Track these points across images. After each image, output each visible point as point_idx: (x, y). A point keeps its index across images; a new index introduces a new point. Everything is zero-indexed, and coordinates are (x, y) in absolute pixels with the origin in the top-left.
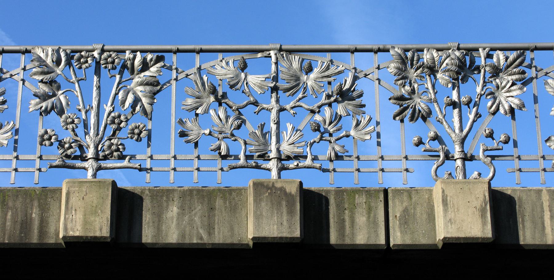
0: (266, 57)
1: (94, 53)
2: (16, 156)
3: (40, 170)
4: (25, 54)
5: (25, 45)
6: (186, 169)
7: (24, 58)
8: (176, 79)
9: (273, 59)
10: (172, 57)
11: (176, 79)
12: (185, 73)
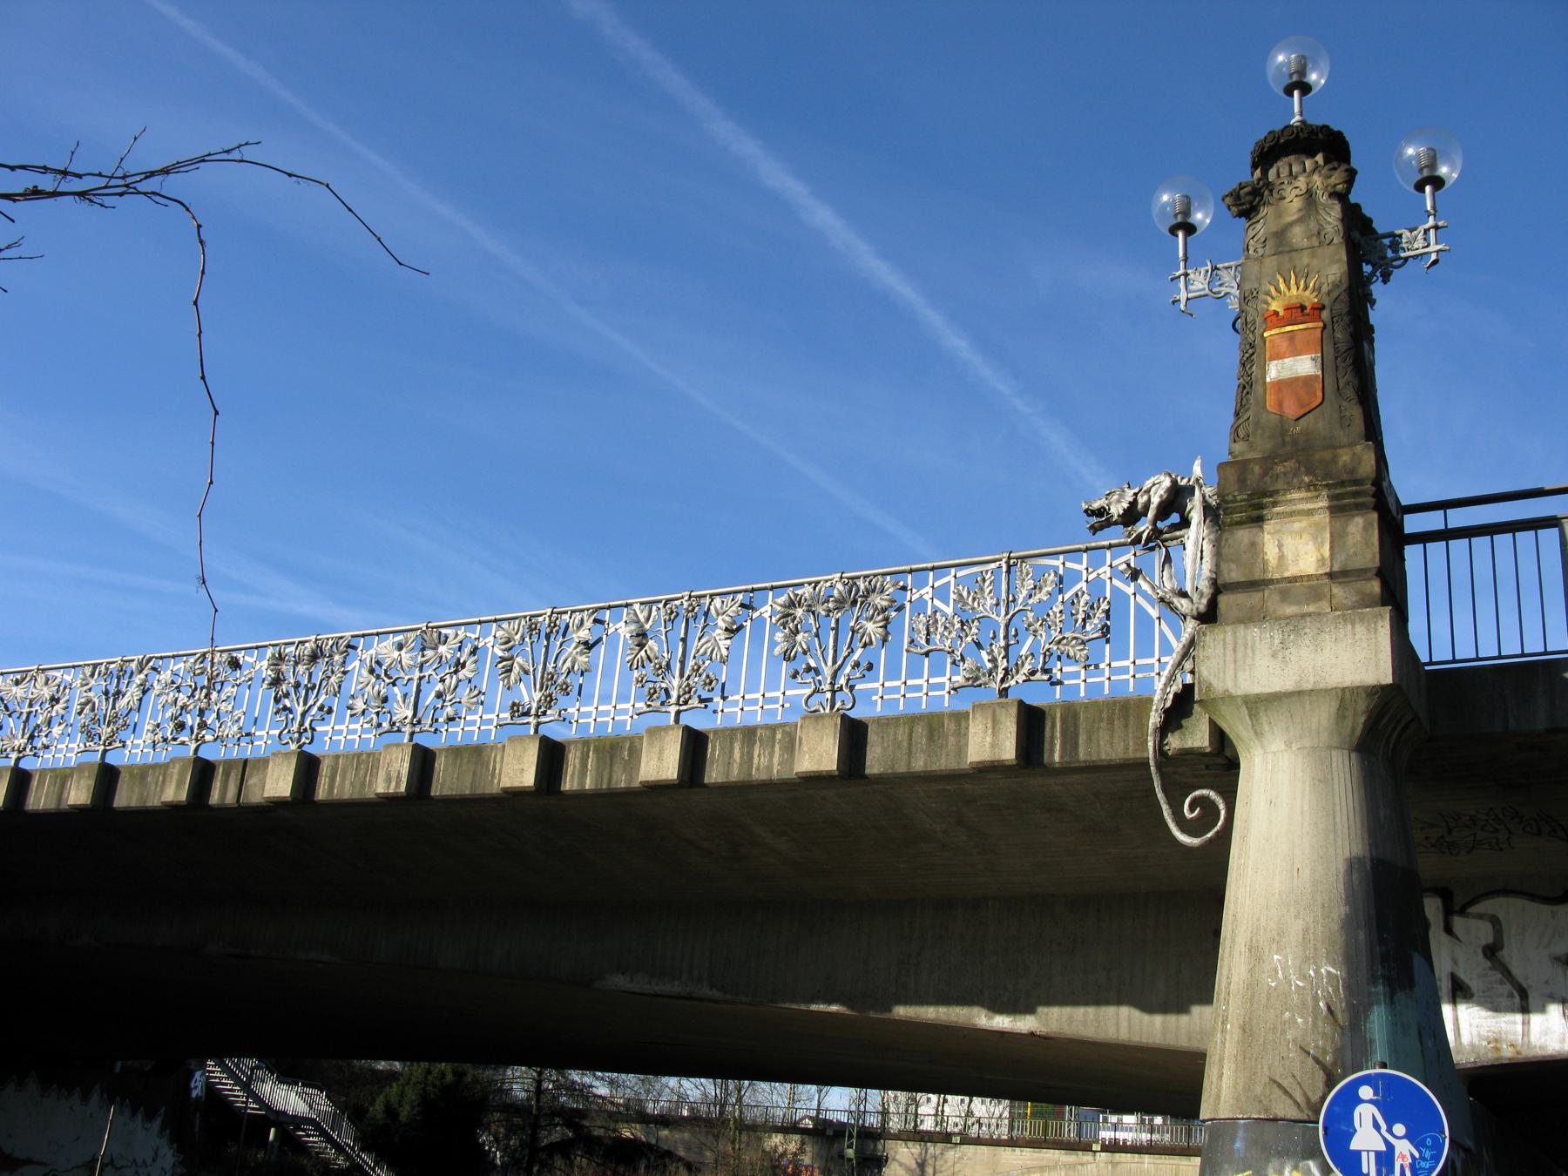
9: (1004, 569)
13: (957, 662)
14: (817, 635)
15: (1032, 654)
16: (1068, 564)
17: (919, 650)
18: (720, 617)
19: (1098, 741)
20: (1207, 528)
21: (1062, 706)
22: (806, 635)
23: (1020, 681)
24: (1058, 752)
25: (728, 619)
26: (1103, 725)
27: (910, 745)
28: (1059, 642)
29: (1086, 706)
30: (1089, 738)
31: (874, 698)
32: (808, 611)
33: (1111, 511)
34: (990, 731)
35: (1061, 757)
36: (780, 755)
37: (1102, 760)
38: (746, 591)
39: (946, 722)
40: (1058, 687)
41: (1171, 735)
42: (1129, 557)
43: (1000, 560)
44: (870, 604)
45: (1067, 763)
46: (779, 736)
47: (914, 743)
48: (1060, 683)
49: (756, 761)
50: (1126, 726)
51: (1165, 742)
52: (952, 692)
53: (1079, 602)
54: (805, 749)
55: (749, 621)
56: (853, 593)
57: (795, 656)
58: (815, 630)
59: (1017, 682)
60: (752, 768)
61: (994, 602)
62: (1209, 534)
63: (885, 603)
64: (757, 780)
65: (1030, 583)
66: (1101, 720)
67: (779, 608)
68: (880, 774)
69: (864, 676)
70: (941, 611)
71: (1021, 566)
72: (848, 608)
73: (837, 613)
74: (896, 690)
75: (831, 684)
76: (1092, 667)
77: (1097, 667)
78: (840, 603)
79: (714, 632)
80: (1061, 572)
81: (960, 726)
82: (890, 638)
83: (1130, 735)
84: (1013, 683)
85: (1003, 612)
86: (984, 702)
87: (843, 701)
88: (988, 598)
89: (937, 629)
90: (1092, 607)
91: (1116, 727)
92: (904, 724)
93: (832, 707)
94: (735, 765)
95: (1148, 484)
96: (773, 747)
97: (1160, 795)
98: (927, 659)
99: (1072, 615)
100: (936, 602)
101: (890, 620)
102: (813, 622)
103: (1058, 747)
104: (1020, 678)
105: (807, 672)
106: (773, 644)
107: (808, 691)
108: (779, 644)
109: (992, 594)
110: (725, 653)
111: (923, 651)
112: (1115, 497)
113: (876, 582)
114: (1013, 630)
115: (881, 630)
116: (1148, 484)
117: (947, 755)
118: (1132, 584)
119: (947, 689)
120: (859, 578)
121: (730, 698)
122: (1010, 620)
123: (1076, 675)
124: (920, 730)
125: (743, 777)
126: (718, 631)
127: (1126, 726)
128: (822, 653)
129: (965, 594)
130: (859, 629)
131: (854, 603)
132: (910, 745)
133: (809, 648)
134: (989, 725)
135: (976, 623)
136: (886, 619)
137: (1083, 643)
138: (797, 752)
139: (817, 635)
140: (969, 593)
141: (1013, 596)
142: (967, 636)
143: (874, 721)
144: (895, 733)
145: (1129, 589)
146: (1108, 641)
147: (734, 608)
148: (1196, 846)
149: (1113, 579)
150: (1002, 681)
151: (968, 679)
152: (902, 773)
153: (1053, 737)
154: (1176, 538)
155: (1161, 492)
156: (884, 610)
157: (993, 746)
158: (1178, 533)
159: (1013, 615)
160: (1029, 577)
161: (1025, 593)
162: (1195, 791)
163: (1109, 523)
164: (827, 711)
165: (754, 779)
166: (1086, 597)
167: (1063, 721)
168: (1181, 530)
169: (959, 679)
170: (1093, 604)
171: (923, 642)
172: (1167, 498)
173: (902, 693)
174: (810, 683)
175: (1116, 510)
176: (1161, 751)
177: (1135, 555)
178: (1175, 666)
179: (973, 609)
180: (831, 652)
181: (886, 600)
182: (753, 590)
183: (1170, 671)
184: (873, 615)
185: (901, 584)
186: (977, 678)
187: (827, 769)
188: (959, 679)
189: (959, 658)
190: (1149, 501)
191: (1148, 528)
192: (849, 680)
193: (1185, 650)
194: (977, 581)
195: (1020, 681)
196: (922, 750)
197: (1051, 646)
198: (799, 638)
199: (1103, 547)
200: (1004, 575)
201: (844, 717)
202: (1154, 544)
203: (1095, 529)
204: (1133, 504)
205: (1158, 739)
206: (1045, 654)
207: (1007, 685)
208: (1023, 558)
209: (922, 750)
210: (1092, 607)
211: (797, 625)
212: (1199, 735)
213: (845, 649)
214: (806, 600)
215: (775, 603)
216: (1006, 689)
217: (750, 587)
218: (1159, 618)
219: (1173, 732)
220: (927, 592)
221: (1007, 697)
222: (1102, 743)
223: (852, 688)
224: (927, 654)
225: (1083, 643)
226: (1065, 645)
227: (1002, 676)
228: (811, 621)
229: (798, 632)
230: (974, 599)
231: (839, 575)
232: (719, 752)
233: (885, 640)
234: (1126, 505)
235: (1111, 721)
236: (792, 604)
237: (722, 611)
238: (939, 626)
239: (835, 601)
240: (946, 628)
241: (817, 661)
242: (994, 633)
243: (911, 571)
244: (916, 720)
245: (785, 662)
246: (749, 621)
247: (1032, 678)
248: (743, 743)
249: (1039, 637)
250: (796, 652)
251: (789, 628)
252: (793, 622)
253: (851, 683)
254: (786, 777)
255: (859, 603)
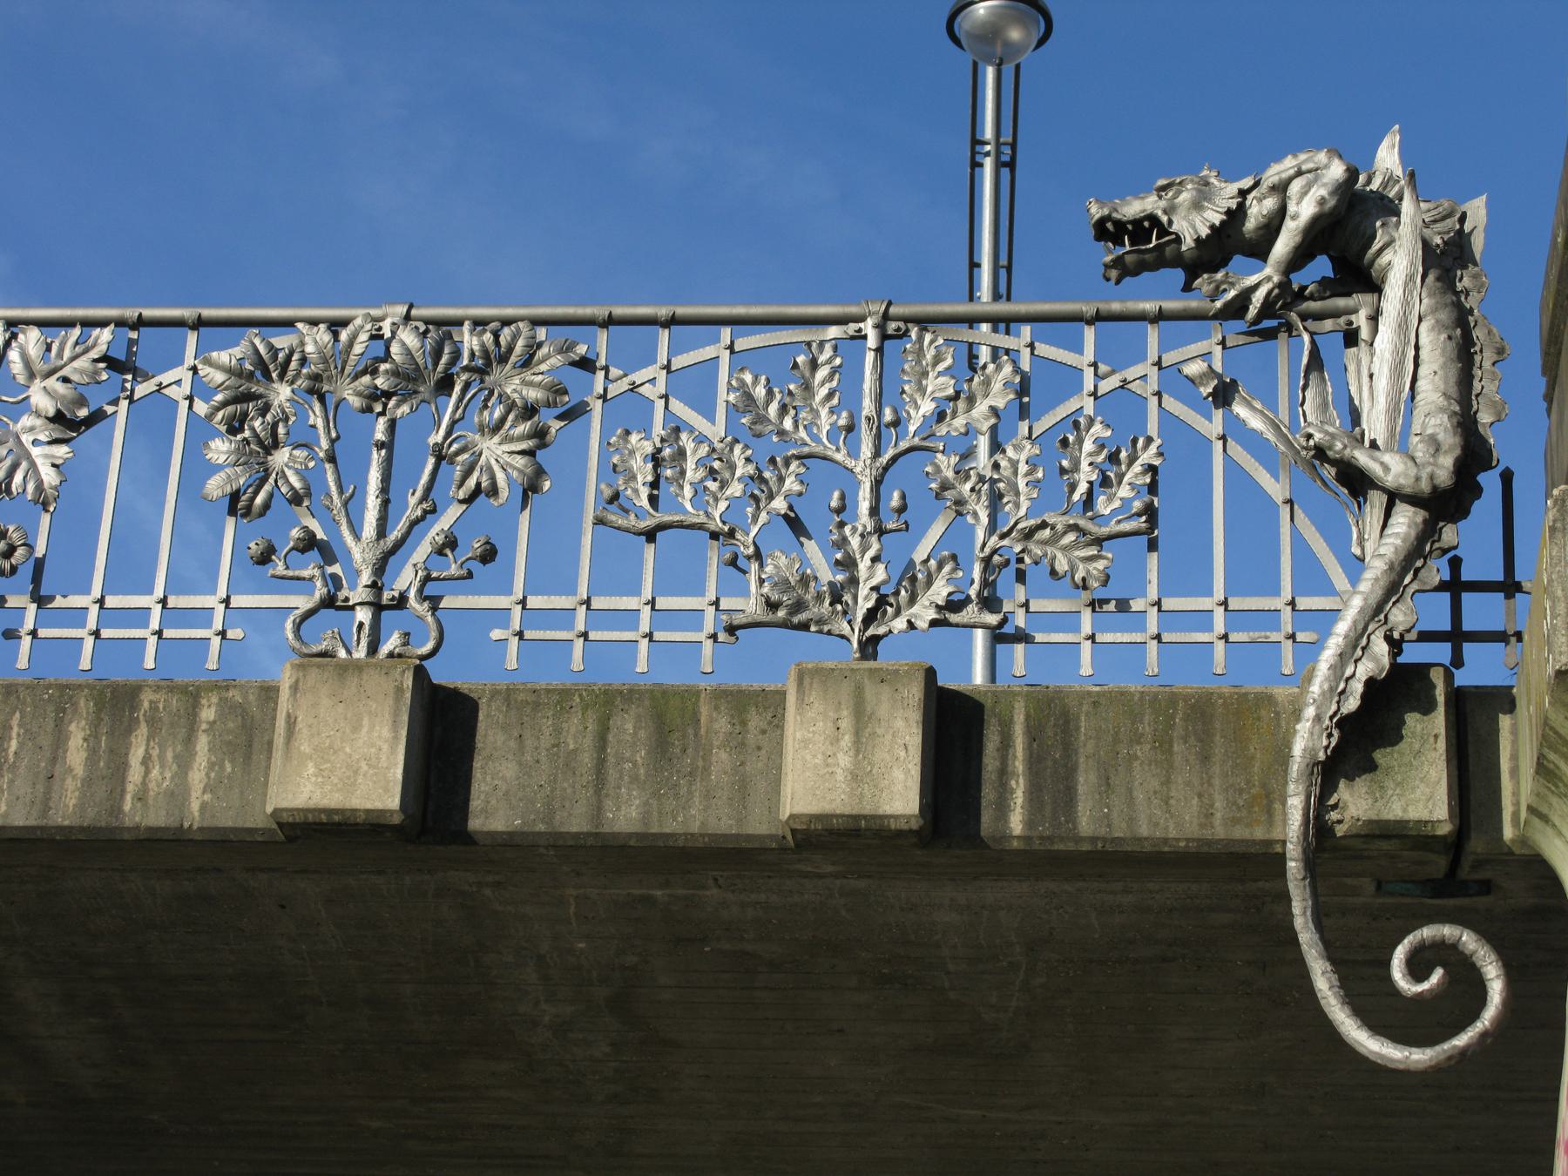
0: (853, 338)
1: (1353, 318)
2: (521, 598)
3: (520, 634)
4: (607, 328)
5: (1157, 299)
6: (550, 635)
7: (605, 337)
8: (604, 397)
9: (872, 342)
10: (595, 337)
11: (604, 397)
12: (626, 380)
13: (741, 562)
14: (332, 458)
15: (954, 557)
16: (1043, 349)
17: (631, 521)
18: (37, 384)
19: (1130, 790)
20: (1429, 295)
21: (1028, 696)
22: (301, 454)
23: (922, 624)
24: (1018, 810)
25: (61, 388)
26: (1143, 751)
27: (601, 764)
28: (1028, 535)
29: (1096, 701)
30: (1106, 782)
31: (496, 634)
32: (311, 391)
33: (1175, 228)
34: (847, 740)
35: (1029, 823)
36: (211, 766)
37: (1140, 840)
38: (120, 323)
39: (704, 711)
40: (1019, 649)
41: (1347, 786)
42: (1211, 344)
43: (862, 319)
44: (491, 393)
45: (1041, 838)
46: (208, 714)
47: (611, 760)
48: (1022, 637)
49: (135, 774)
50: (1205, 759)
51: (1332, 802)
52: (722, 637)
53: (1080, 441)
54: (305, 748)
55: (124, 404)
56: (444, 359)
57: (267, 506)
58: (325, 444)
59: (911, 625)
60: (123, 792)
61: (842, 422)
62: (1434, 310)
63: (533, 395)
64: (137, 828)
65: (939, 384)
66: (1137, 739)
67: (219, 377)
68: (511, 834)
69: (470, 575)
70: (692, 430)
71: (920, 339)
72: (426, 396)
73: (398, 406)
74: (563, 617)
75: (374, 585)
76: (1112, 606)
77: (1123, 606)
78: (409, 379)
79: (16, 421)
80: (1025, 365)
81: (744, 723)
82: (547, 485)
83: (1217, 781)
84: (900, 624)
85: (866, 450)
86: (830, 664)
87: (407, 634)
88: (824, 412)
89: (683, 473)
90: (1113, 458)
91: (1178, 759)
92: (585, 709)
93: (373, 649)
94: (69, 781)
95: (1273, 174)
96: (189, 740)
97: (1307, 937)
98: (650, 550)
99: (1063, 471)
100: (677, 406)
101: (549, 438)
102: (320, 423)
103: (1019, 797)
104: (923, 613)
105: (303, 551)
106: (197, 468)
107: (303, 603)
108: (219, 468)
109: (835, 401)
110: (49, 476)
111: (644, 524)
112: (1185, 197)
113: (515, 337)
114: (896, 495)
115: (520, 461)
116: (1273, 174)
117: (708, 796)
118: (1218, 415)
119: (709, 627)
120: (459, 323)
121: (59, 602)
122: (886, 469)
123: (1068, 621)
124: (628, 726)
125: (91, 817)
126: (27, 421)
127: (1205, 759)
128: (345, 504)
129: (760, 392)
130: (458, 453)
131: (445, 385)
132: (601, 764)
133: (307, 488)
134: (846, 723)
135: (794, 466)
136: (540, 434)
137: (1099, 541)
138: (278, 755)
139: (332, 458)
140: (770, 393)
141: (895, 411)
142: (771, 497)
143: (495, 693)
144: (558, 731)
145: (1213, 425)
146: (1153, 546)
147: (83, 363)
148: (1421, 1066)
149: (1165, 397)
150: (871, 617)
151: (772, 606)
152: (577, 835)
153: (1004, 773)
154: (1335, 314)
155: (1319, 192)
156: (529, 411)
157: (855, 777)
158: (1341, 302)
159: (894, 459)
160: (941, 367)
161: (927, 407)
162: (1421, 926)
163: (1160, 261)
164: (360, 653)
165: (128, 823)
166: (1098, 429)
167: (1033, 735)
168: (1349, 295)
169: (750, 605)
170: (1118, 451)
171: (645, 503)
172: (1335, 207)
173: (581, 627)
174: (311, 579)
175: (1192, 226)
176: (1319, 829)
177: (1223, 343)
178: (1370, 612)
179: (782, 433)
180: (372, 503)
181: (539, 385)
182: (140, 323)
183: (1355, 623)
184: (503, 420)
185: (582, 349)
186: (799, 606)
187: (369, 806)
188: (750, 605)
189: (751, 550)
190: (1281, 213)
191: (1269, 279)
192: (427, 579)
193: (1393, 576)
194: (795, 366)
195: (922, 624)
196: (635, 779)
197: (1006, 542)
198: (281, 457)
199: (1141, 317)
200: (870, 357)
201: (420, 673)
202: (1273, 323)
203: (1124, 270)
204: (1236, 215)
205: (1316, 790)
206: (987, 561)
207: (881, 630)
208: (924, 322)
209: (635, 779)
210: (1113, 458)
211: (275, 426)
212: (1422, 790)
213: (413, 501)
214: (304, 361)
215: (208, 362)
216: (876, 639)
217: (131, 313)
218: (1290, 502)
219: (1351, 778)
220: (651, 380)
221: (875, 660)
222: (1140, 796)
223: (434, 602)
224: (650, 535)
225: (1099, 541)
226: (1045, 543)
227: (870, 604)
228: (316, 418)
229: (276, 444)
230: (783, 409)
231: (403, 310)
232: (21, 745)
233: (531, 488)
234: (1217, 218)
235: (1163, 744)
236: (263, 368)
237: (46, 367)
238: (690, 464)
239: (395, 373)
240: (713, 473)
241: (331, 524)
242: (843, 497)
243: (610, 322)
244: (618, 701)
245: (230, 523)
246: (124, 404)
247: (954, 618)
248: (95, 725)
249: (970, 519)
250: (271, 496)
251: (253, 429)
252: (264, 416)
253: (431, 589)
254: (230, 824)
255: (457, 388)
